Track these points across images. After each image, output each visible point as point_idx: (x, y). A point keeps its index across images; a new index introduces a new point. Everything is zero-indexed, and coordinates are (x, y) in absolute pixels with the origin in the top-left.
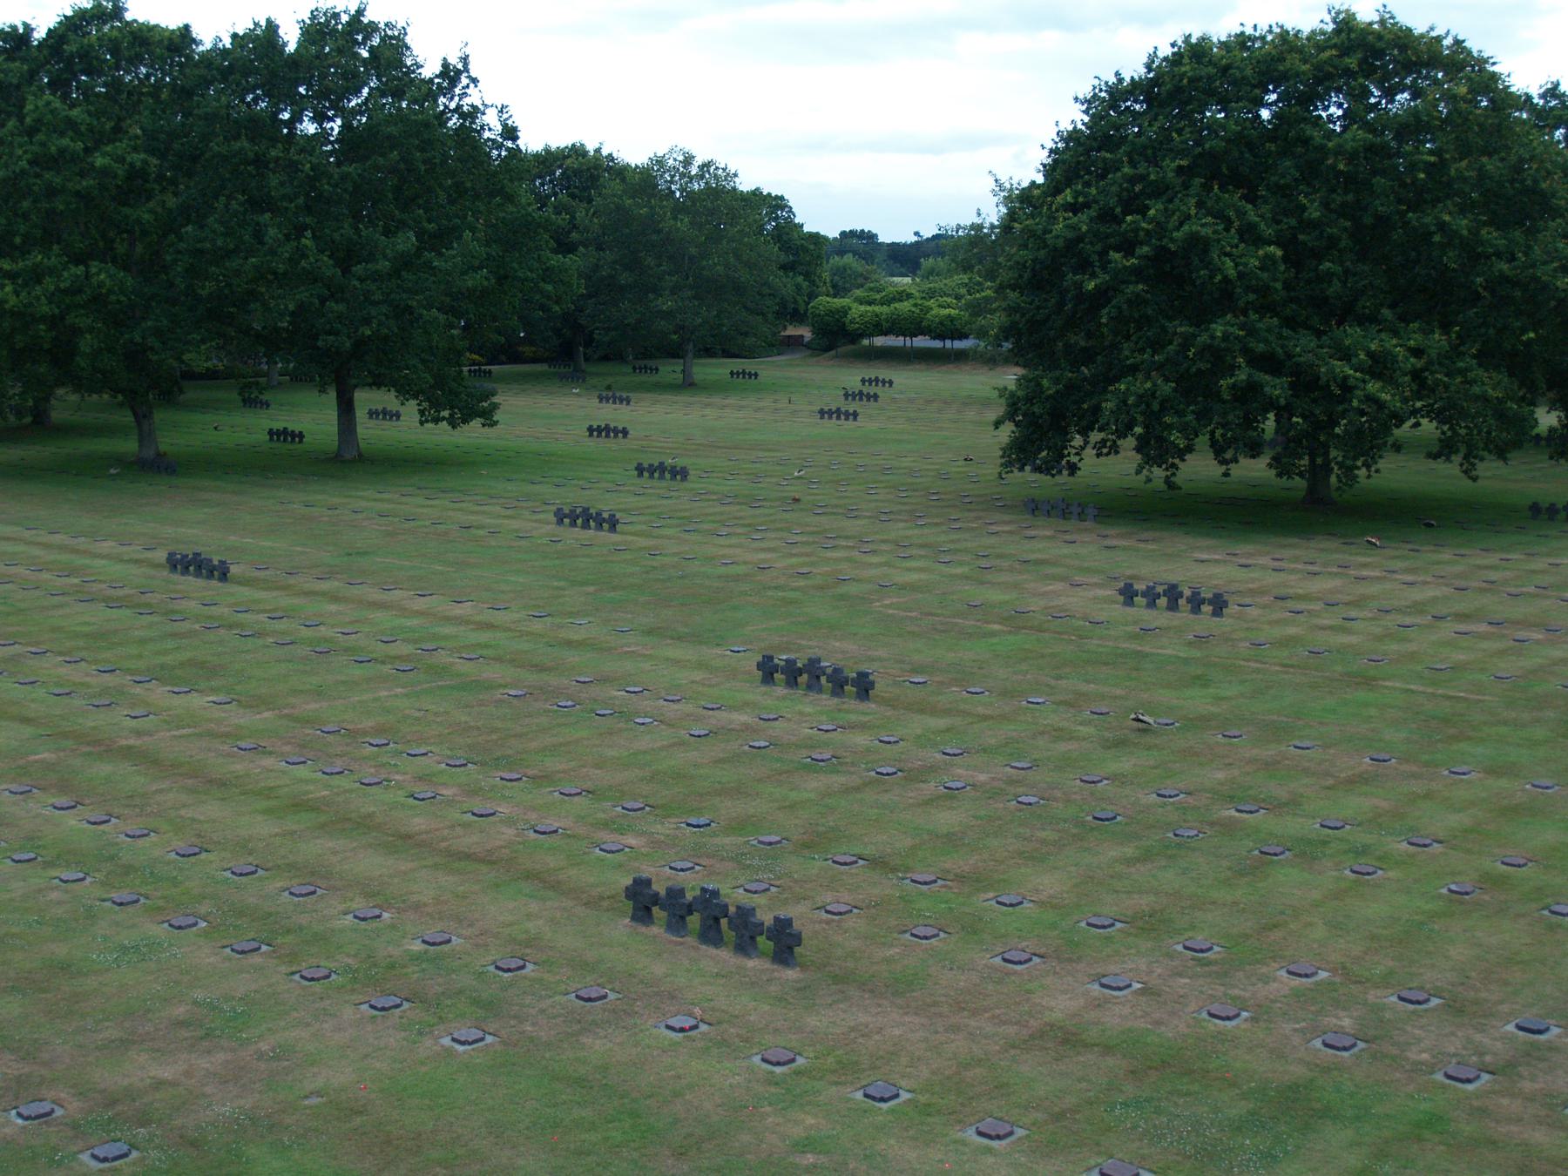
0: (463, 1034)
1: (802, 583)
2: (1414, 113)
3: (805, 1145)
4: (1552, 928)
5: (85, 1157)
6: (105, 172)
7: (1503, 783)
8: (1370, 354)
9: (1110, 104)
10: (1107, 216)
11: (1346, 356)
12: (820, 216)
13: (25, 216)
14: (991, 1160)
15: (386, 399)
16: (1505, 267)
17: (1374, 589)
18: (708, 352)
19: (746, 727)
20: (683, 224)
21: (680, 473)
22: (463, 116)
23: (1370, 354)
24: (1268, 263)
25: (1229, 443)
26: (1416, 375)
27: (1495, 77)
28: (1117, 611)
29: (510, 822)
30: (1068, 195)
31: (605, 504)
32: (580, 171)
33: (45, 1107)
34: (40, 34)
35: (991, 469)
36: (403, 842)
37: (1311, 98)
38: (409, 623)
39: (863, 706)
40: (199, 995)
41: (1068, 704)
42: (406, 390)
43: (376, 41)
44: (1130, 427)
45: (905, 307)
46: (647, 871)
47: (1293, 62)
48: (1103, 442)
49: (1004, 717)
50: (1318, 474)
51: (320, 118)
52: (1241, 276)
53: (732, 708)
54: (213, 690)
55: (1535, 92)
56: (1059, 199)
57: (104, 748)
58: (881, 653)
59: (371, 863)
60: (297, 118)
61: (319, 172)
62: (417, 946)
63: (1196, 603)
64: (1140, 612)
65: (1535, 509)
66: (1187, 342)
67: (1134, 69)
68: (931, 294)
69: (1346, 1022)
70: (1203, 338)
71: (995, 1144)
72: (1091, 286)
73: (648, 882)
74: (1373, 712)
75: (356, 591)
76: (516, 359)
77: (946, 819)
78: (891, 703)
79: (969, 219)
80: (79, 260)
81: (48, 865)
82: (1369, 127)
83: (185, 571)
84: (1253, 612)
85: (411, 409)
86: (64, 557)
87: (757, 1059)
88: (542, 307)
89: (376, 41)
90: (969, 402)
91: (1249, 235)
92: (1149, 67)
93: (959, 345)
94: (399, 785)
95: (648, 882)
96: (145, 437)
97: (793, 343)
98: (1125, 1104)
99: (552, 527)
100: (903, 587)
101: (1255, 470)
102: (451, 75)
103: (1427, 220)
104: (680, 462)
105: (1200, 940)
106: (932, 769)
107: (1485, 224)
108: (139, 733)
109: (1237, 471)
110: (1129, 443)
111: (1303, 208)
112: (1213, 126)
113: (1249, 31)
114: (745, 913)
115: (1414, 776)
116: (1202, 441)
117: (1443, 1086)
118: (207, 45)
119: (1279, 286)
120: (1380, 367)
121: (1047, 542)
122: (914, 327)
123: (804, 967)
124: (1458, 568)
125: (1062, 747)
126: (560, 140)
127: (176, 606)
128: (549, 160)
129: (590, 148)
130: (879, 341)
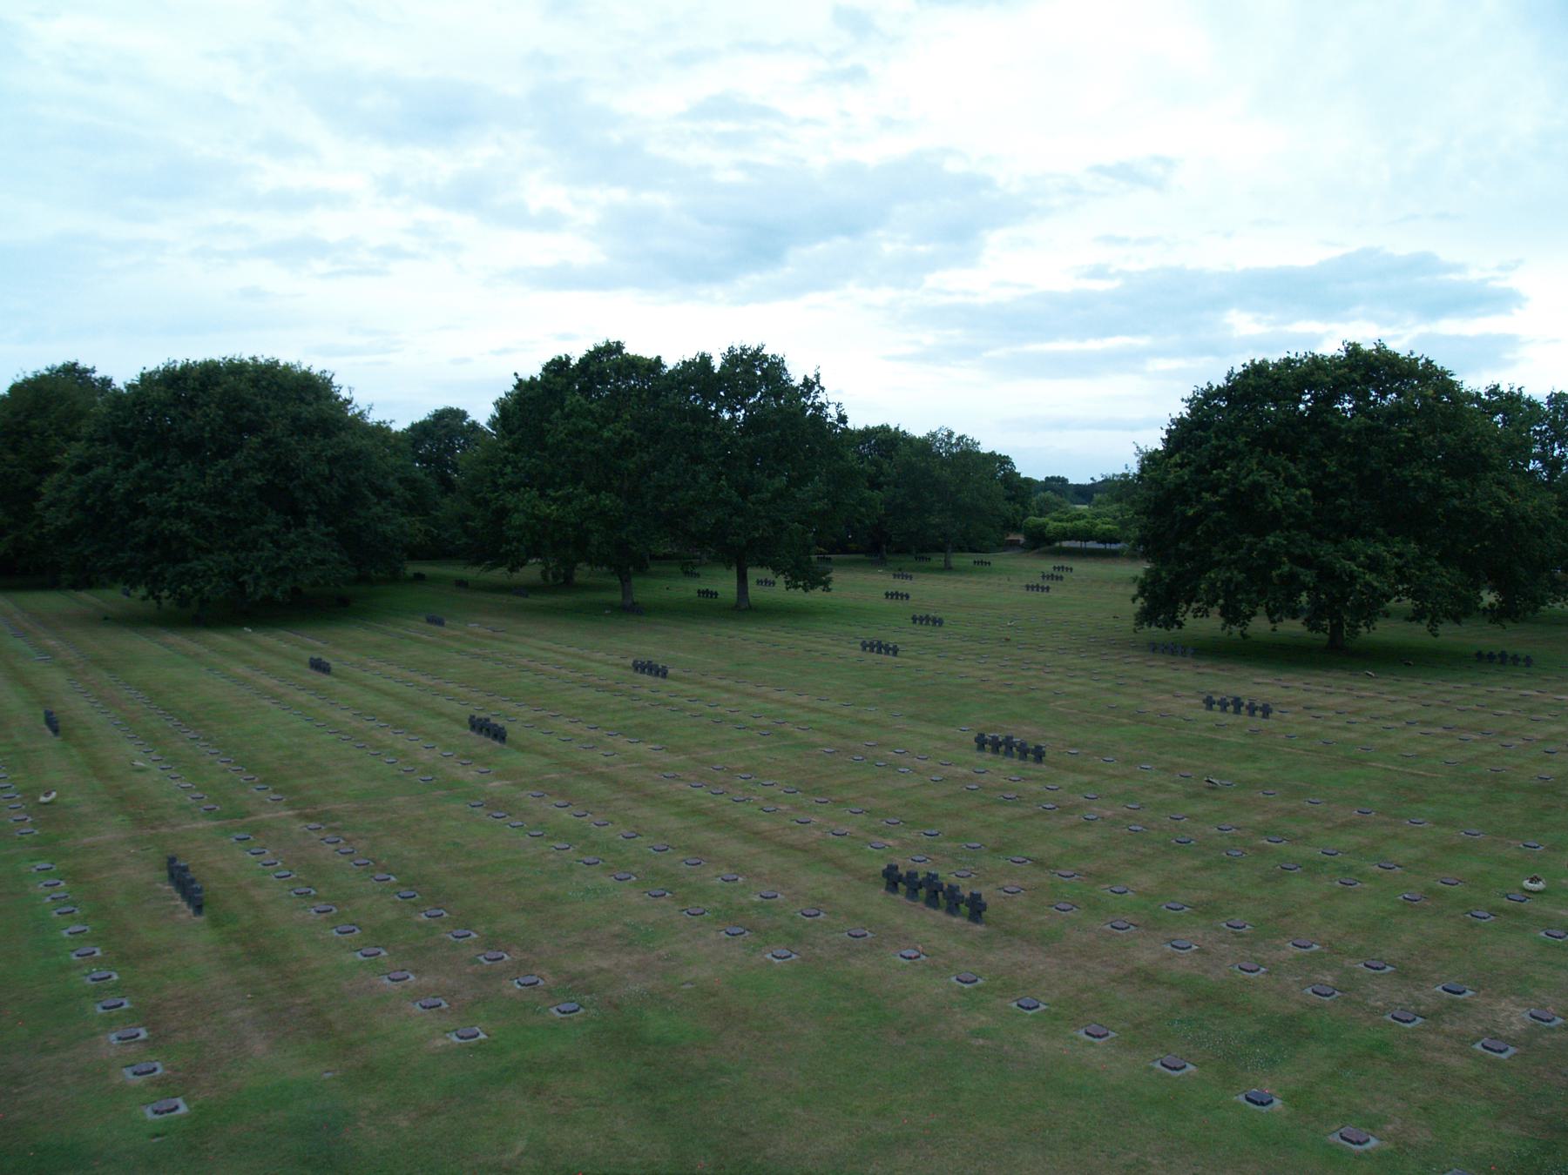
0: (778, 952)
1: (1007, 690)
2: (1397, 405)
3: (977, 1034)
4: (1472, 926)
5: (553, 1010)
6: (609, 440)
7: (1445, 830)
8: (1368, 557)
9: (1204, 403)
10: (1201, 470)
11: (1352, 557)
12: (1031, 467)
13: (563, 465)
14: (1092, 1050)
15: (767, 573)
16: (1456, 502)
17: (1369, 704)
18: (960, 549)
19: (966, 777)
20: (947, 472)
21: (938, 622)
22: (816, 408)
23: (1368, 557)
24: (1302, 499)
25: (1277, 610)
26: (1398, 569)
27: (1453, 383)
28: (1203, 712)
29: (818, 827)
30: (1177, 458)
31: (891, 639)
32: (885, 441)
33: (534, 979)
34: (574, 362)
35: (1130, 623)
36: (757, 836)
37: (1335, 396)
38: (769, 706)
39: (1038, 766)
40: (627, 920)
41: (1166, 770)
42: (777, 569)
43: (765, 365)
44: (1215, 601)
45: (1081, 523)
46: (898, 860)
47: (1319, 376)
48: (1199, 610)
49: (1125, 776)
50: (1336, 629)
51: (733, 410)
52: (1285, 507)
53: (958, 765)
54: (653, 742)
55: (1482, 391)
56: (1172, 461)
57: (588, 773)
58: (1052, 734)
59: (734, 848)
60: (719, 409)
61: (733, 441)
62: (757, 899)
63: (1252, 709)
64: (1216, 714)
65: (1479, 655)
66: (1251, 548)
67: (1219, 381)
68: (1098, 516)
69: (1329, 978)
70: (1262, 545)
71: (1096, 1040)
72: (1191, 513)
74: (1362, 781)
75: (740, 687)
76: (846, 551)
77: (1084, 838)
79: (1120, 471)
80: (592, 490)
81: (551, 839)
82: (1370, 416)
83: (643, 671)
84: (1289, 716)
85: (781, 581)
86: (575, 661)
87: (953, 979)
88: (859, 521)
89: (765, 365)
91: (1291, 482)
92: (1228, 379)
93: (1114, 547)
94: (755, 803)
96: (627, 594)
97: (1013, 545)
98: (1181, 1021)
99: (859, 652)
100: (1068, 694)
101: (1293, 627)
102: (809, 385)
103: (1406, 473)
104: (939, 615)
105: (1237, 921)
106: (1078, 806)
107: (1446, 475)
108: (608, 765)
109: (1281, 627)
110: (1216, 609)
111: (1325, 465)
112: (1269, 415)
113: (1292, 356)
114: (953, 890)
115: (1386, 823)
116: (1261, 610)
117: (1391, 1024)
118: (670, 367)
119: (1309, 513)
120: (1374, 564)
121: (1161, 670)
122: (1087, 536)
123: (988, 924)
124: (1425, 692)
125: (1161, 796)
126: (874, 423)
127: (636, 691)
128: (868, 434)
129: (892, 427)
130: (1066, 544)
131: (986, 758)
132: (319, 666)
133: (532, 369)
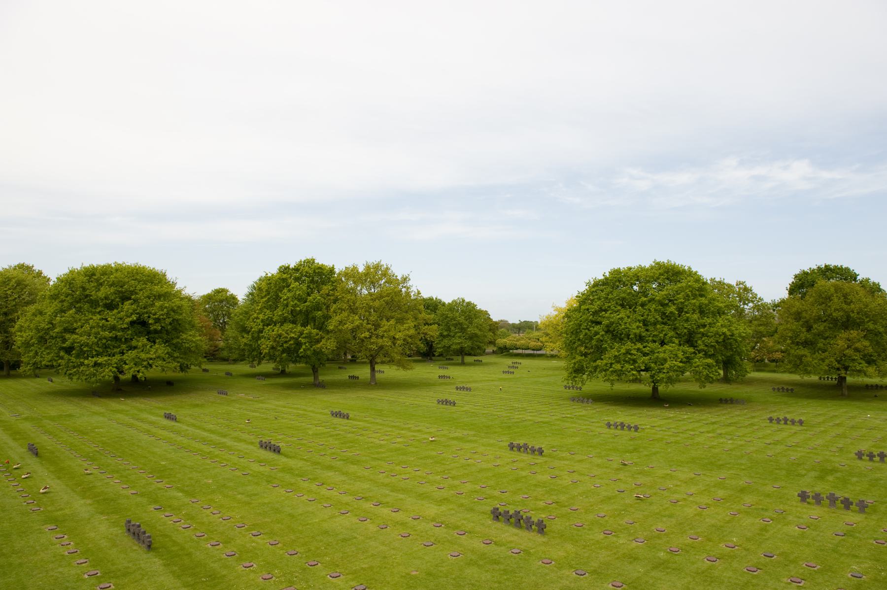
12: (495, 317)
64: (612, 431)
73: (498, 509)
78: (550, 456)
90: (557, 369)
95: (498, 509)
96: (316, 378)
130: (515, 351)
131: (515, 455)
132: (169, 417)
133: (273, 270)
